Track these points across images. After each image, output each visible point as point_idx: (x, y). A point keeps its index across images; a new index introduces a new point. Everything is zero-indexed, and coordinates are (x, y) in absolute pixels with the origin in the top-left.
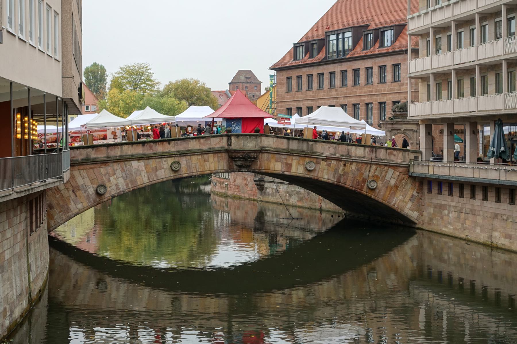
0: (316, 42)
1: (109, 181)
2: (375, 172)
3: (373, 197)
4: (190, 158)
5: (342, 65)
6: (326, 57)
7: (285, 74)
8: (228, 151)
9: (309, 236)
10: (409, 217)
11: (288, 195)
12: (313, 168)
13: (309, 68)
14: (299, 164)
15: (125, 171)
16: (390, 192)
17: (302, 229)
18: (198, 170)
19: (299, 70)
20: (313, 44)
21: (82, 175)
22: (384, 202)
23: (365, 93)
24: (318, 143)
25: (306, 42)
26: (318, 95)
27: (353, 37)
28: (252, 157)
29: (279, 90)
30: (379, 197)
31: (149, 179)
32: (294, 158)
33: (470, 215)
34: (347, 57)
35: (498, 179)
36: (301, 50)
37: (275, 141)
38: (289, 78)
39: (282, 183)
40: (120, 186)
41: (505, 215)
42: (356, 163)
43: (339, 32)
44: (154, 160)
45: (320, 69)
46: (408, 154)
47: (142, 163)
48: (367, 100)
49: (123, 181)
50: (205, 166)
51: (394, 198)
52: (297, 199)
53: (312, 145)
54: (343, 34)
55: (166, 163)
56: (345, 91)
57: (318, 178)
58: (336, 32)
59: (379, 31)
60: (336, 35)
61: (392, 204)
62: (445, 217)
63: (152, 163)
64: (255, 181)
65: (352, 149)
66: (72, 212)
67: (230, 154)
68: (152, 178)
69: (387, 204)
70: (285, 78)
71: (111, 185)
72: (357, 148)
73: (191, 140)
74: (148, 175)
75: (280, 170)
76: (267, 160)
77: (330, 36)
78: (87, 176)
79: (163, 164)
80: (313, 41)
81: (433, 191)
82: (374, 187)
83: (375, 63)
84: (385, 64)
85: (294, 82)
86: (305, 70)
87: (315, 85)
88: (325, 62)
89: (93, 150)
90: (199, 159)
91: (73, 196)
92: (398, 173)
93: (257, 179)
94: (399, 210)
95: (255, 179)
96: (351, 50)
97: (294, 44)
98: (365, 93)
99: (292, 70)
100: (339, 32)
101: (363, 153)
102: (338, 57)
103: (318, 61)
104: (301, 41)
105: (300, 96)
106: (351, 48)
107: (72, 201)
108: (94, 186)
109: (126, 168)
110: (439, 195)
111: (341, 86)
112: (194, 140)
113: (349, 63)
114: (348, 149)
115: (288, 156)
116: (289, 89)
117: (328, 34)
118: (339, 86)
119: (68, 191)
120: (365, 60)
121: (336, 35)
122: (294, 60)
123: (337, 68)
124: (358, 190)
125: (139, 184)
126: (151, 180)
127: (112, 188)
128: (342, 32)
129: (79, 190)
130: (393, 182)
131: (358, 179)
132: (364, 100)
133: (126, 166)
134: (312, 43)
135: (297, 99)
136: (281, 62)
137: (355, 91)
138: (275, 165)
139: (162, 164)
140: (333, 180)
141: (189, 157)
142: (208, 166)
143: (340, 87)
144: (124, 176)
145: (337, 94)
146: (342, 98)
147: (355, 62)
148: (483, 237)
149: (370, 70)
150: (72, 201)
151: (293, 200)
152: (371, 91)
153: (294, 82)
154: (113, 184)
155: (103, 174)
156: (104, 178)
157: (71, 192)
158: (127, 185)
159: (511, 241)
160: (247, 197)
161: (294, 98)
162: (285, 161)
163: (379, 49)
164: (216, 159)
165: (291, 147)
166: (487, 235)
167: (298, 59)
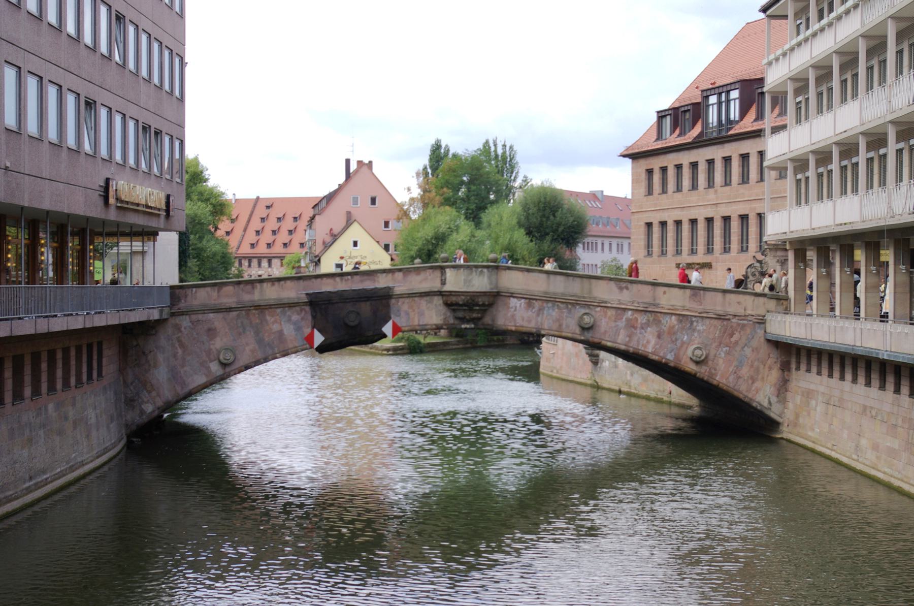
0: (689, 107)
6: (701, 134)
7: (645, 164)
8: (440, 293)
20: (685, 111)
25: (674, 109)
28: (481, 303)
33: (838, 408)
34: (731, 133)
36: (668, 121)
38: (650, 172)
41: (874, 408)
43: (721, 90)
54: (728, 92)
57: (599, 341)
67: (444, 298)
70: (644, 171)
77: (731, 92)
80: (684, 106)
82: (703, 358)
85: (657, 177)
87: (686, 182)
88: (699, 143)
96: (737, 122)
97: (658, 112)
100: (721, 90)
106: (737, 119)
110: (807, 374)
112: (384, 275)
122: (657, 139)
123: (717, 153)
128: (725, 89)
146: (724, 204)
153: (657, 177)
167: (664, 137)
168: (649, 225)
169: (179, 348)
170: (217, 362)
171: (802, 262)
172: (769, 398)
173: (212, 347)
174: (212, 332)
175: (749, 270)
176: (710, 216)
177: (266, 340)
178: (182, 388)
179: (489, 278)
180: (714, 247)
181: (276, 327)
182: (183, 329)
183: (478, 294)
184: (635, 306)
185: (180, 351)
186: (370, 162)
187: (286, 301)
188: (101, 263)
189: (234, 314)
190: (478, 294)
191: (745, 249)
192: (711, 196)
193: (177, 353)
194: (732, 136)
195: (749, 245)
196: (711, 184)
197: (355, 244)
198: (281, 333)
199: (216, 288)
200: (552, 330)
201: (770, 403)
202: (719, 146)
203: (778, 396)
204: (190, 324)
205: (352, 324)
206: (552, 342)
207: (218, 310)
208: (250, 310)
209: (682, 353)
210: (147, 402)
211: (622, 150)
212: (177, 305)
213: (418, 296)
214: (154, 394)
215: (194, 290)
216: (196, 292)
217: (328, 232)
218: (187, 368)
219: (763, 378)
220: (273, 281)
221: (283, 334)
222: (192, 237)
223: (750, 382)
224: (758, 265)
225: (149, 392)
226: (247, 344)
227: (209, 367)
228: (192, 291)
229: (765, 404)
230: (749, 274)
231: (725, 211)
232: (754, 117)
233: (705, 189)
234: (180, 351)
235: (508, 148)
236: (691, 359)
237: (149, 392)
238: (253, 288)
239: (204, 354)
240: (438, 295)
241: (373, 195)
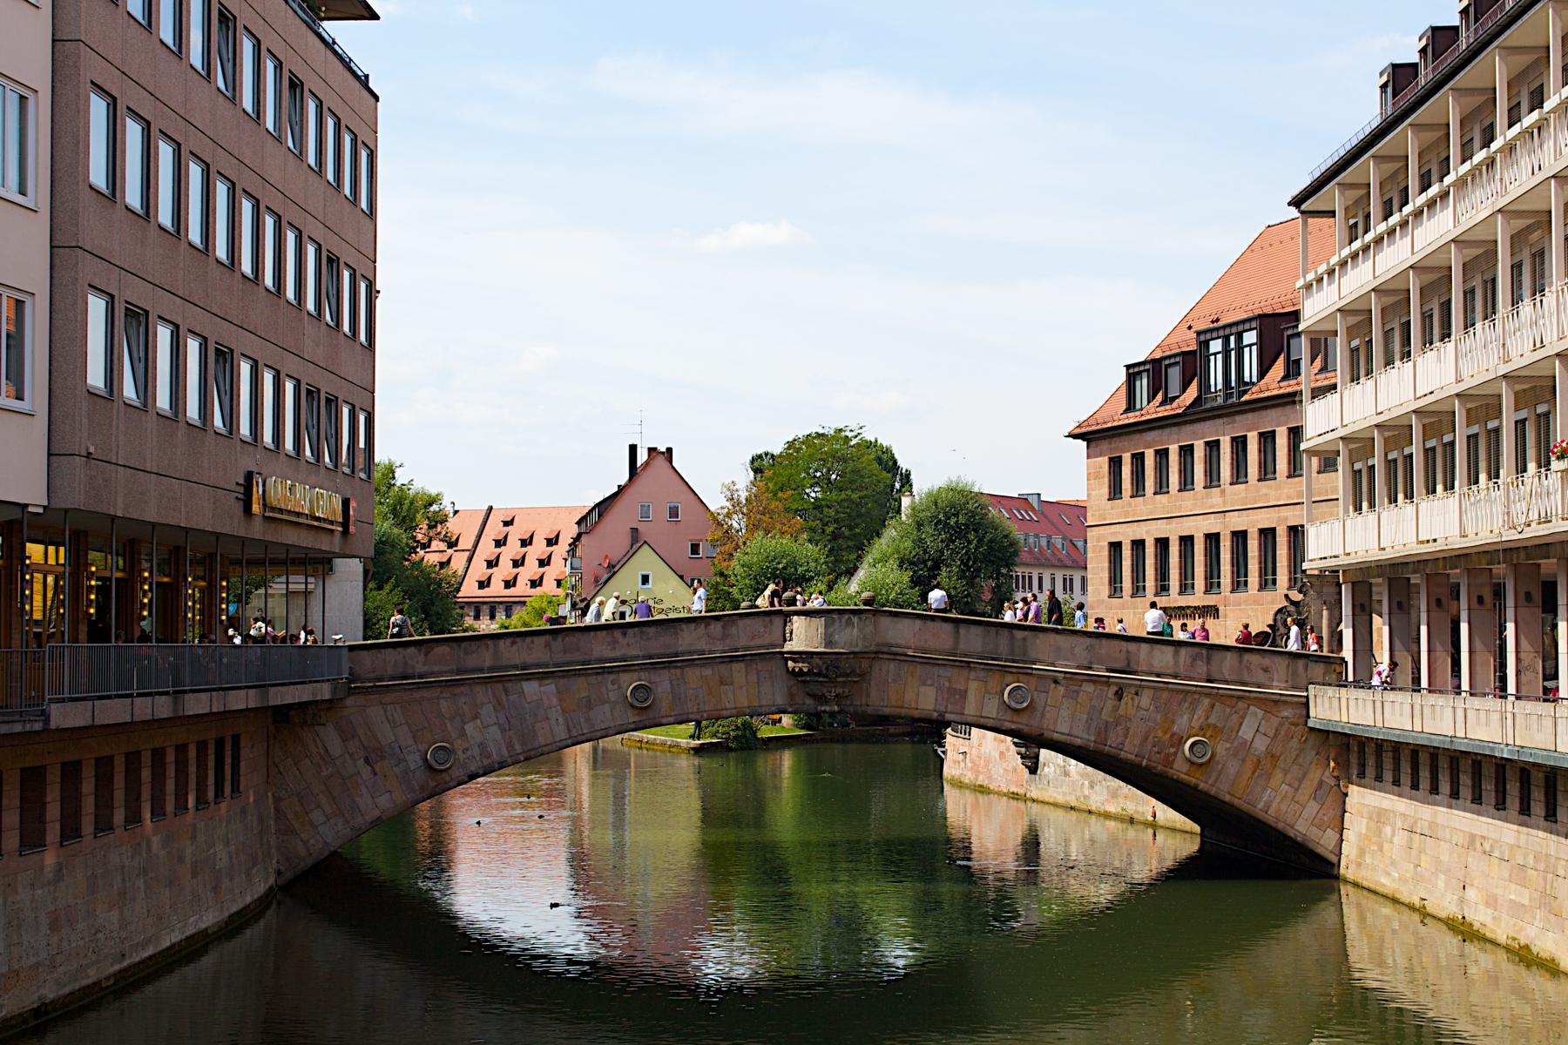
1: (463, 734)
2: (1207, 718)
3: (1202, 786)
4: (682, 674)
5: (1234, 422)
6: (1198, 401)
10: (1311, 845)
11: (1086, 782)
12: (1025, 705)
13: (1160, 431)
14: (987, 692)
15: (504, 708)
16: (1253, 773)
18: (702, 707)
19: (1137, 436)
21: (390, 718)
22: (1236, 802)
23: (1288, 498)
24: (1041, 635)
26: (1180, 506)
27: (1261, 343)
29: (1094, 493)
30: (1221, 787)
31: (569, 731)
32: (973, 675)
34: (1246, 398)
35: (1451, 733)
36: (1143, 384)
37: (917, 629)
40: (492, 748)
42: (1152, 691)
43: (1227, 331)
44: (583, 678)
45: (1185, 436)
46: (1306, 669)
47: (550, 687)
49: (498, 735)
50: (723, 697)
51: (1264, 789)
53: (1024, 639)
55: (616, 686)
56: (1243, 495)
58: (1221, 333)
60: (1220, 341)
61: (1260, 806)
62: (1386, 846)
63: (581, 687)
65: (1139, 650)
66: (362, 815)
68: (578, 727)
69: (1245, 807)
71: (466, 745)
72: (1153, 649)
73: (684, 626)
74: (566, 720)
75: (931, 708)
76: (895, 680)
78: (403, 721)
79: (608, 691)
86: (1150, 436)
88: (1198, 413)
89: (420, 651)
90: (706, 676)
91: (366, 771)
92: (1275, 721)
94: (1280, 826)
96: (1254, 384)
97: (1128, 367)
98: (1288, 498)
99: (1123, 438)
100: (1227, 331)
101: (1171, 662)
102: (1226, 400)
107: (363, 787)
108: (420, 747)
109: (508, 700)
114: (1128, 652)
115: (956, 670)
116: (1115, 492)
117: (1202, 338)
119: (355, 760)
121: (1220, 341)
124: (1160, 767)
125: (543, 743)
126: (574, 733)
127: (469, 753)
128: (1234, 330)
129: (383, 758)
130: (1261, 745)
131: (1160, 733)
132: (1286, 519)
133: (507, 695)
134: (1167, 362)
135: (1133, 516)
137: (1266, 494)
138: (918, 695)
139: (604, 690)
140: (1085, 736)
141: (679, 671)
142: (730, 695)
143: (1231, 484)
144: (501, 721)
145: (1224, 503)
147: (1264, 413)
148: (1445, 903)
150: (363, 787)
154: (472, 742)
155: (447, 716)
156: (448, 725)
157: (361, 762)
158: (510, 745)
159: (1496, 914)
160: (1005, 791)
161: (1126, 514)
162: (947, 684)
164: (753, 677)
165: (962, 646)
166: (1455, 897)
197: (645, 579)
206: (963, 735)
211: (1071, 427)
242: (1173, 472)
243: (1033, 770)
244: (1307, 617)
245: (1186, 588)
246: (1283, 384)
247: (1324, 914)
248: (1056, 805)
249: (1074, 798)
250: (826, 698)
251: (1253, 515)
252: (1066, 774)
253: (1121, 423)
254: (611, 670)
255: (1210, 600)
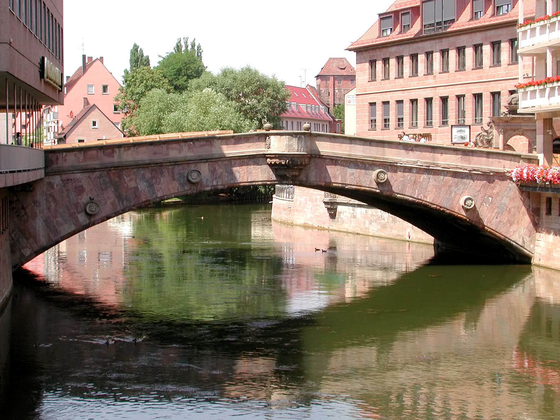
5: (442, 42)
9: (393, 276)
17: (385, 269)
34: (449, 30)
39: (359, 206)
45: (413, 48)
48: (477, 89)
52: (379, 227)
59: (399, 13)
64: (325, 203)
81: (553, 212)
83: (486, 38)
84: (500, 40)
86: (393, 49)
93: (327, 200)
95: (325, 201)
97: (380, 15)
103: (410, 37)
104: (389, 11)
105: (387, 85)
111: (426, 73)
113: (451, 39)
118: (438, 71)
120: (473, 34)
132: (471, 90)
136: (362, 39)
145: (436, 82)
146: (442, 88)
149: (480, 47)
151: (374, 229)
152: (481, 77)
163: (491, 19)
168: (373, 104)
169: (52, 203)
170: (83, 213)
171: (549, 129)
172: (523, 238)
173: (79, 201)
174: (80, 190)
175: (478, 138)
176: (429, 96)
177: (124, 194)
178: (55, 235)
179: (305, 143)
180: (433, 121)
181: (132, 184)
182: (55, 186)
183: (300, 156)
184: (419, 165)
185: (53, 205)
186: (102, 58)
187: (140, 162)
188: (25, 130)
189: (97, 174)
190: (300, 156)
191: (414, 125)
192: (430, 81)
193: (51, 206)
194: (451, 32)
195: (418, 122)
196: (387, 77)
197: (94, 124)
198: (136, 188)
199: (82, 152)
200: (354, 185)
201: (524, 242)
202: (437, 41)
203: (530, 237)
204: (61, 182)
205: (193, 181)
206: (282, 199)
207: (85, 170)
208: (110, 170)
209: (455, 202)
210: (27, 247)
211: (348, 45)
212: (51, 166)
213: (247, 158)
214: (31, 240)
215: (64, 154)
216: (66, 155)
217: (69, 115)
218: (60, 219)
219: (518, 222)
220: (128, 147)
221: (138, 189)
222: (246, 90)
223: (509, 225)
224: (486, 134)
225: (27, 239)
226: (109, 198)
227: (77, 217)
228: (63, 154)
229: (520, 243)
230: (478, 141)
231: (444, 92)
232: (469, 17)
233: (424, 75)
234: (53, 205)
235: (196, 48)
236: (463, 207)
237: (27, 239)
238: (113, 152)
239: (73, 207)
240: (262, 157)
241: (105, 84)
242: (406, 67)
243: (333, 216)
244: (492, 138)
245: (414, 125)
246: (471, 22)
247: (528, 281)
248: (348, 233)
249: (359, 229)
250: (287, 177)
251: (451, 89)
252: (355, 217)
253: (377, 43)
254: (456, 151)
255: (427, 131)
